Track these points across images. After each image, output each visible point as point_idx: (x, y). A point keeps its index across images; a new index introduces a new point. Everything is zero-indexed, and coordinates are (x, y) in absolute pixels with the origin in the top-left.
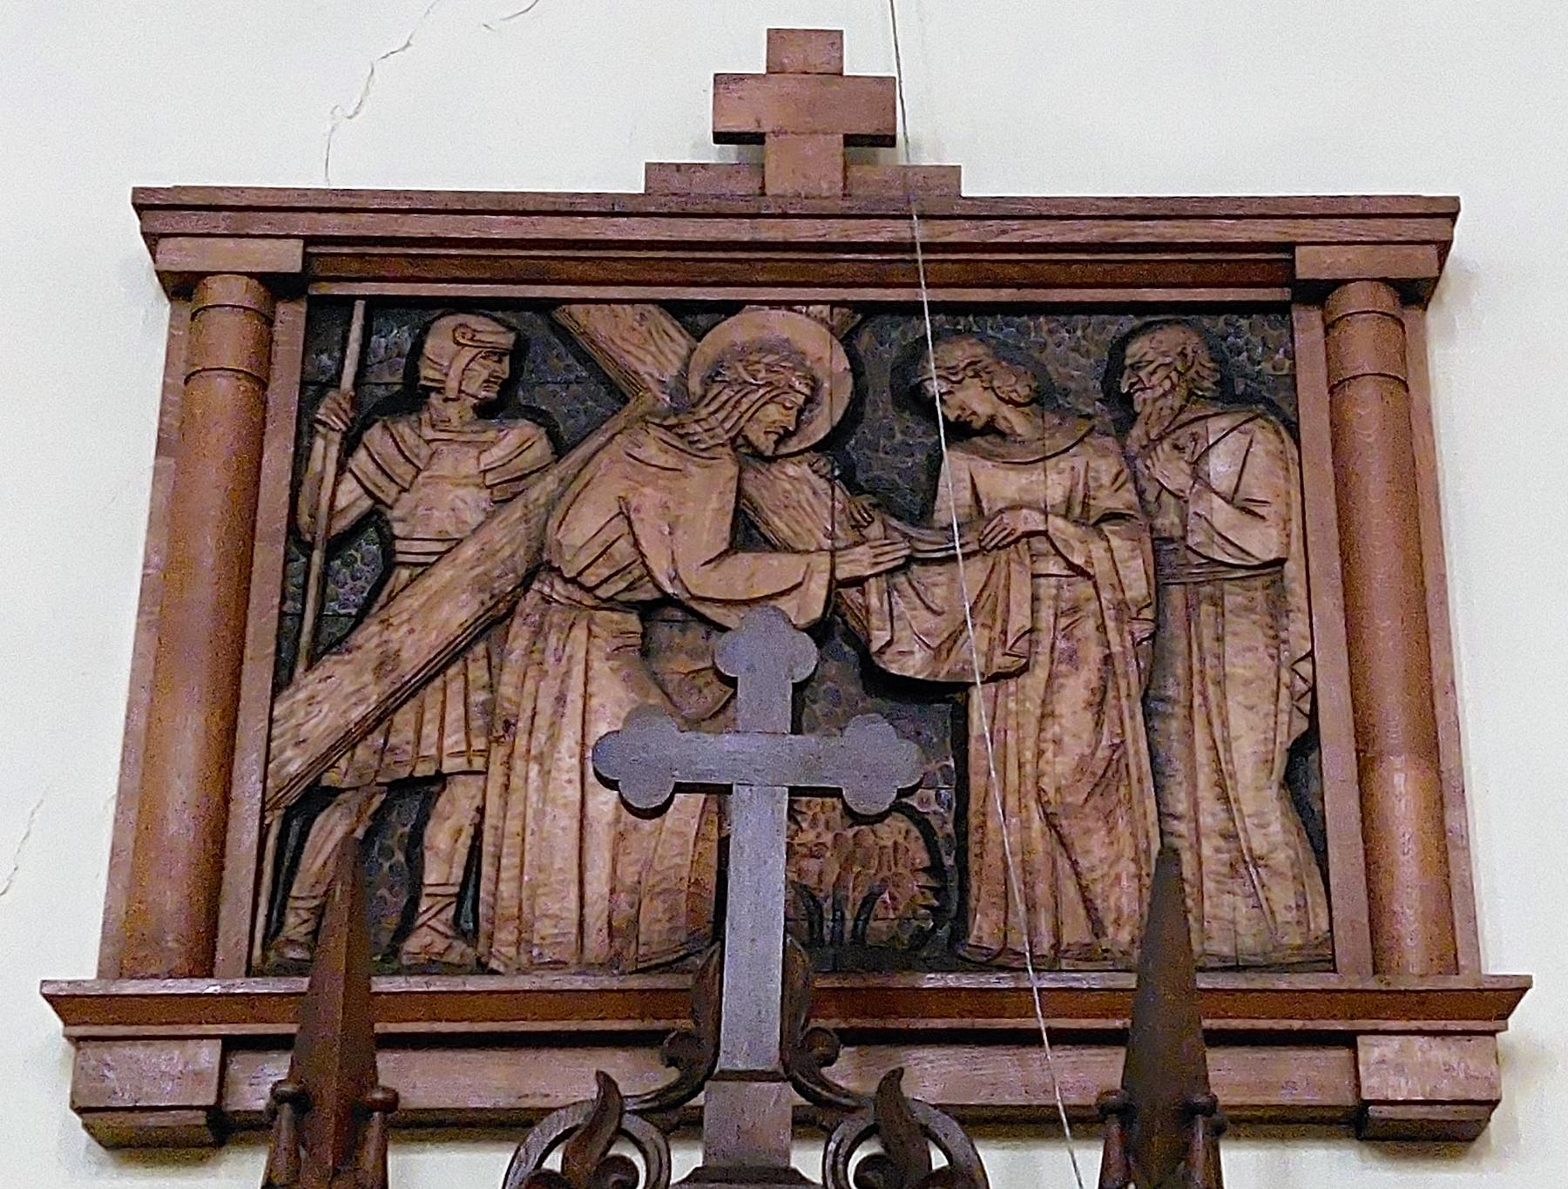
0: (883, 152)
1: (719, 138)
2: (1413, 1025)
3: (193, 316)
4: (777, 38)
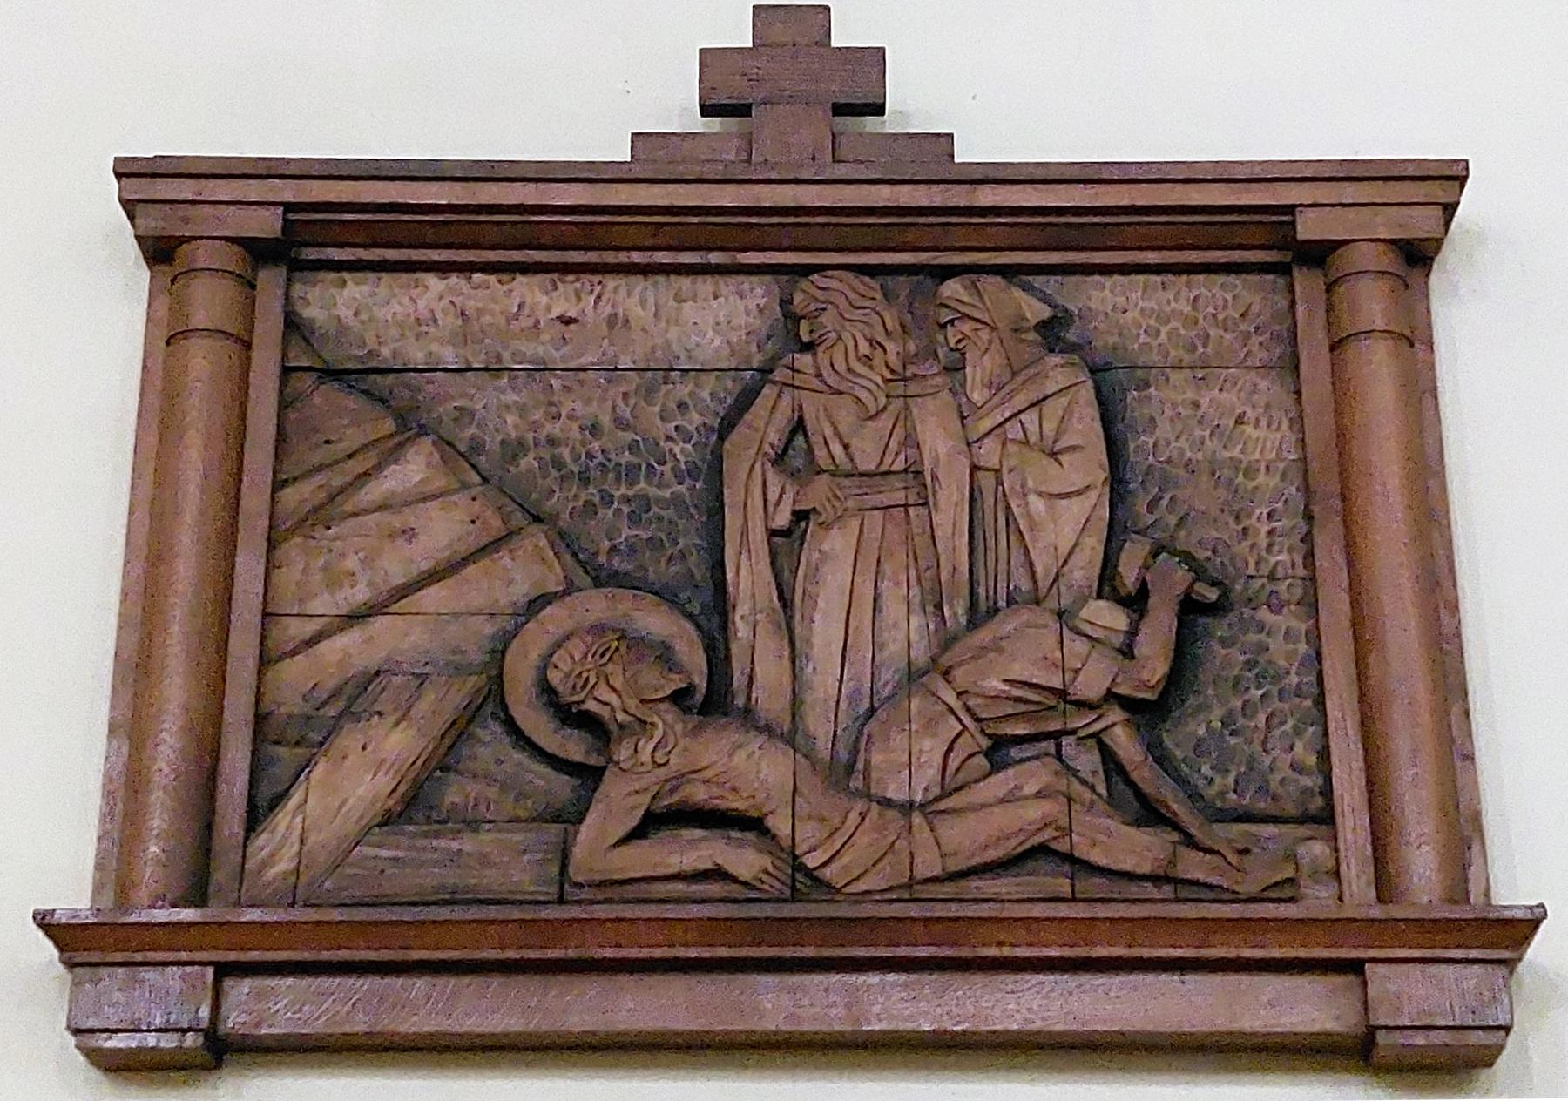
0: (870, 123)
2: (1474, 954)
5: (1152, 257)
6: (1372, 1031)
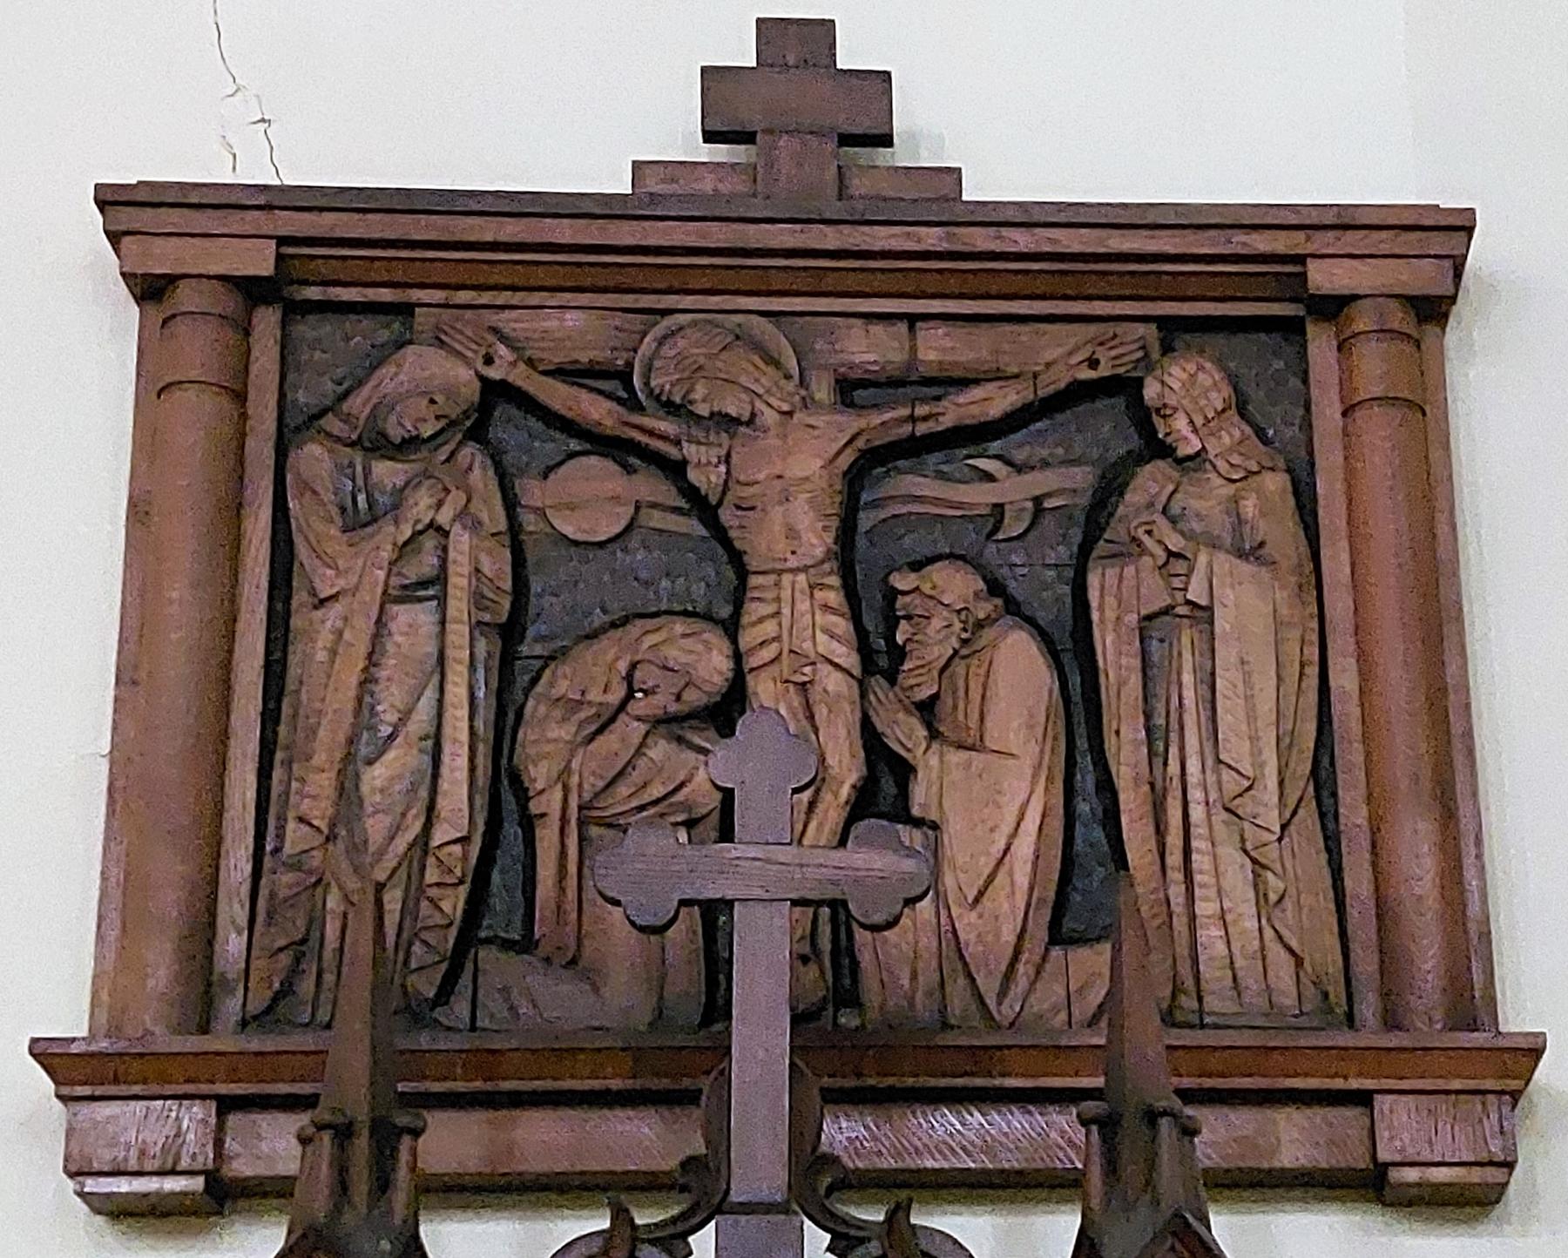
0: (882, 156)
1: (710, 137)
3: (165, 322)
4: (768, 29)
5: (952, 306)
6: (1382, 1169)
